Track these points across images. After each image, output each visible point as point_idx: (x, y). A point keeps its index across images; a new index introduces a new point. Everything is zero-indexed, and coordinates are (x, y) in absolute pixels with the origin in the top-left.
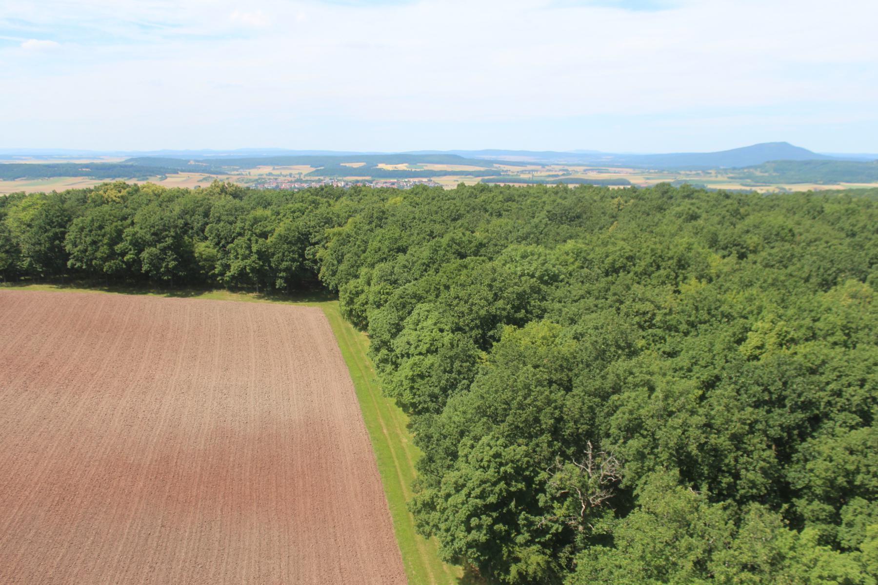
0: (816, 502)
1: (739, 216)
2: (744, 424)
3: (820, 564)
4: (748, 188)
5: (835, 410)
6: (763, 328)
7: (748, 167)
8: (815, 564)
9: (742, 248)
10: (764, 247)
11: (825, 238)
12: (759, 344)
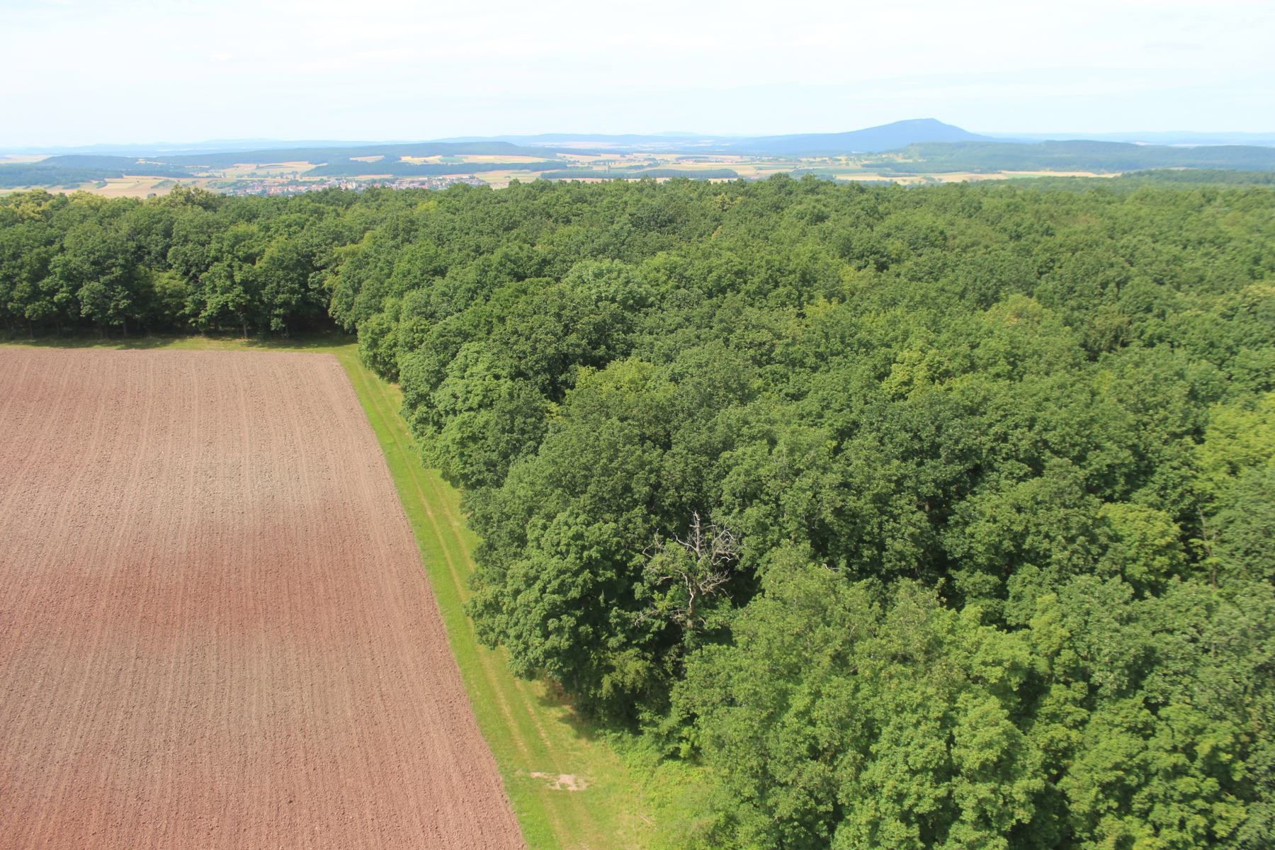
0: (979, 573)
1: (876, 216)
2: (890, 481)
3: (983, 647)
4: (888, 179)
5: (999, 458)
6: (910, 358)
7: (888, 152)
8: (977, 649)
9: (882, 256)
10: (909, 255)
11: (984, 242)
12: (906, 378)
